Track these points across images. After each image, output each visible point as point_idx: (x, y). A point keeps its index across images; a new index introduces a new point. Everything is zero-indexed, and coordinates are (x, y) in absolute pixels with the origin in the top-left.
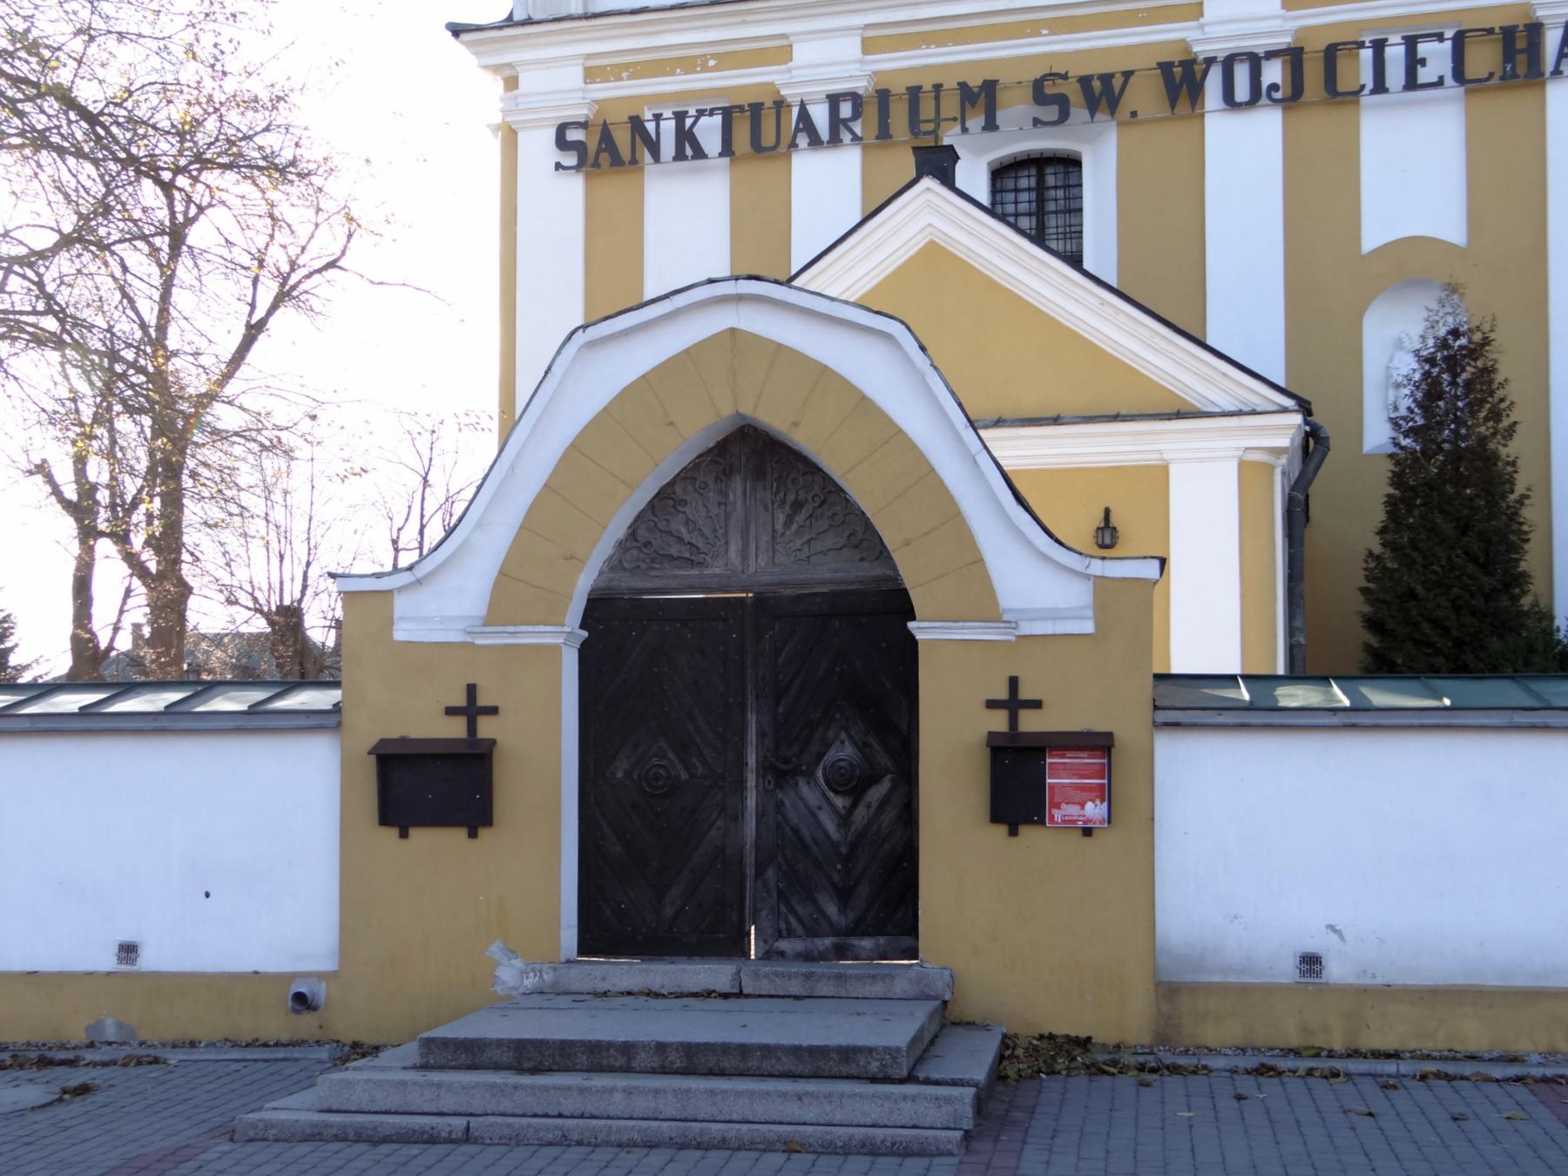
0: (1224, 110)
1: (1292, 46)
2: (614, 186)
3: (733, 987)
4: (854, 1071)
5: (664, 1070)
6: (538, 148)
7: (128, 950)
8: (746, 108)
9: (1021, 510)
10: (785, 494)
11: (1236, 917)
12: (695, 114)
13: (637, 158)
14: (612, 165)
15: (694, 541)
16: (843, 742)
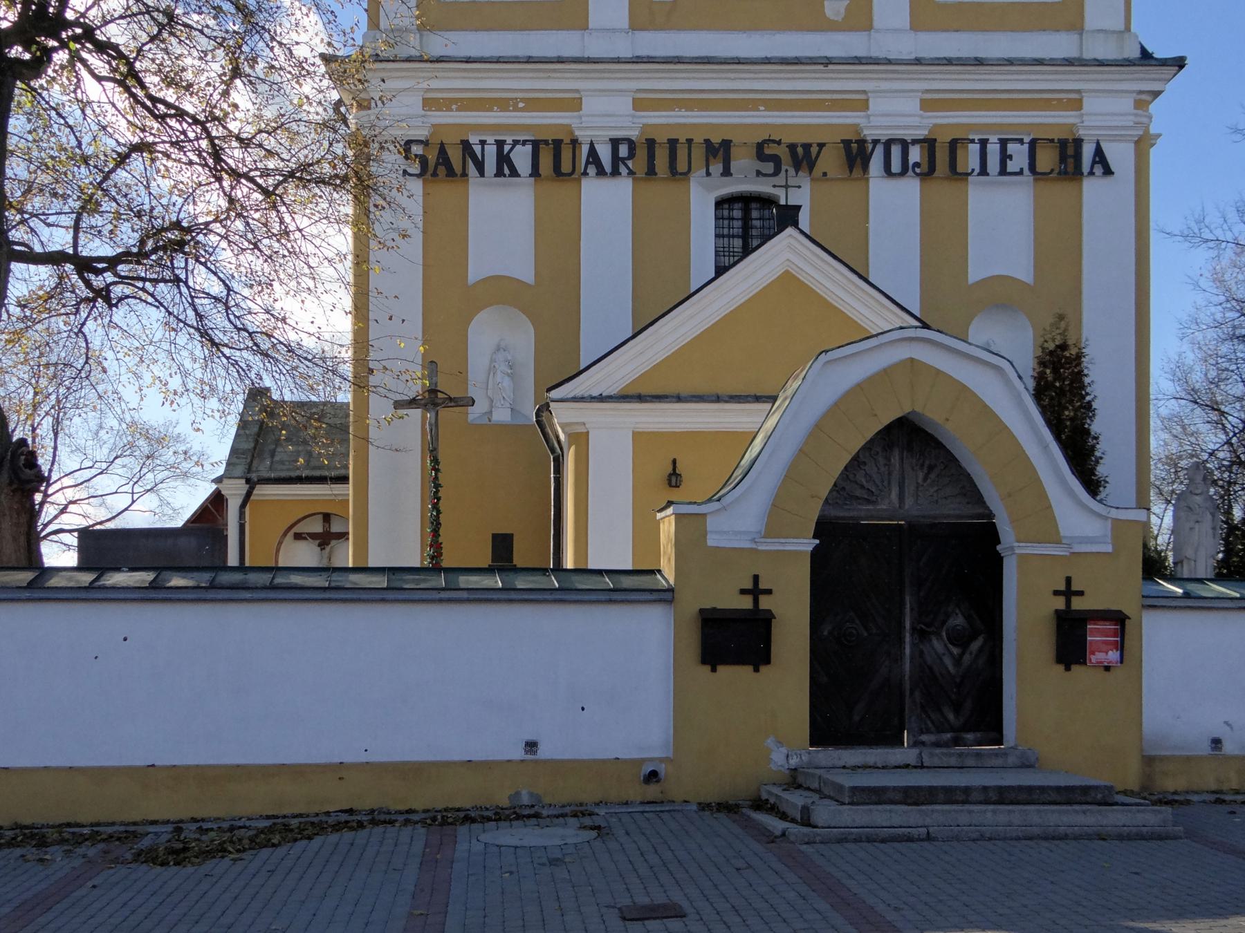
0: (883, 177)
2: (446, 190)
3: (917, 762)
4: (1089, 800)
5: (987, 802)
7: (531, 746)
16: (957, 614)
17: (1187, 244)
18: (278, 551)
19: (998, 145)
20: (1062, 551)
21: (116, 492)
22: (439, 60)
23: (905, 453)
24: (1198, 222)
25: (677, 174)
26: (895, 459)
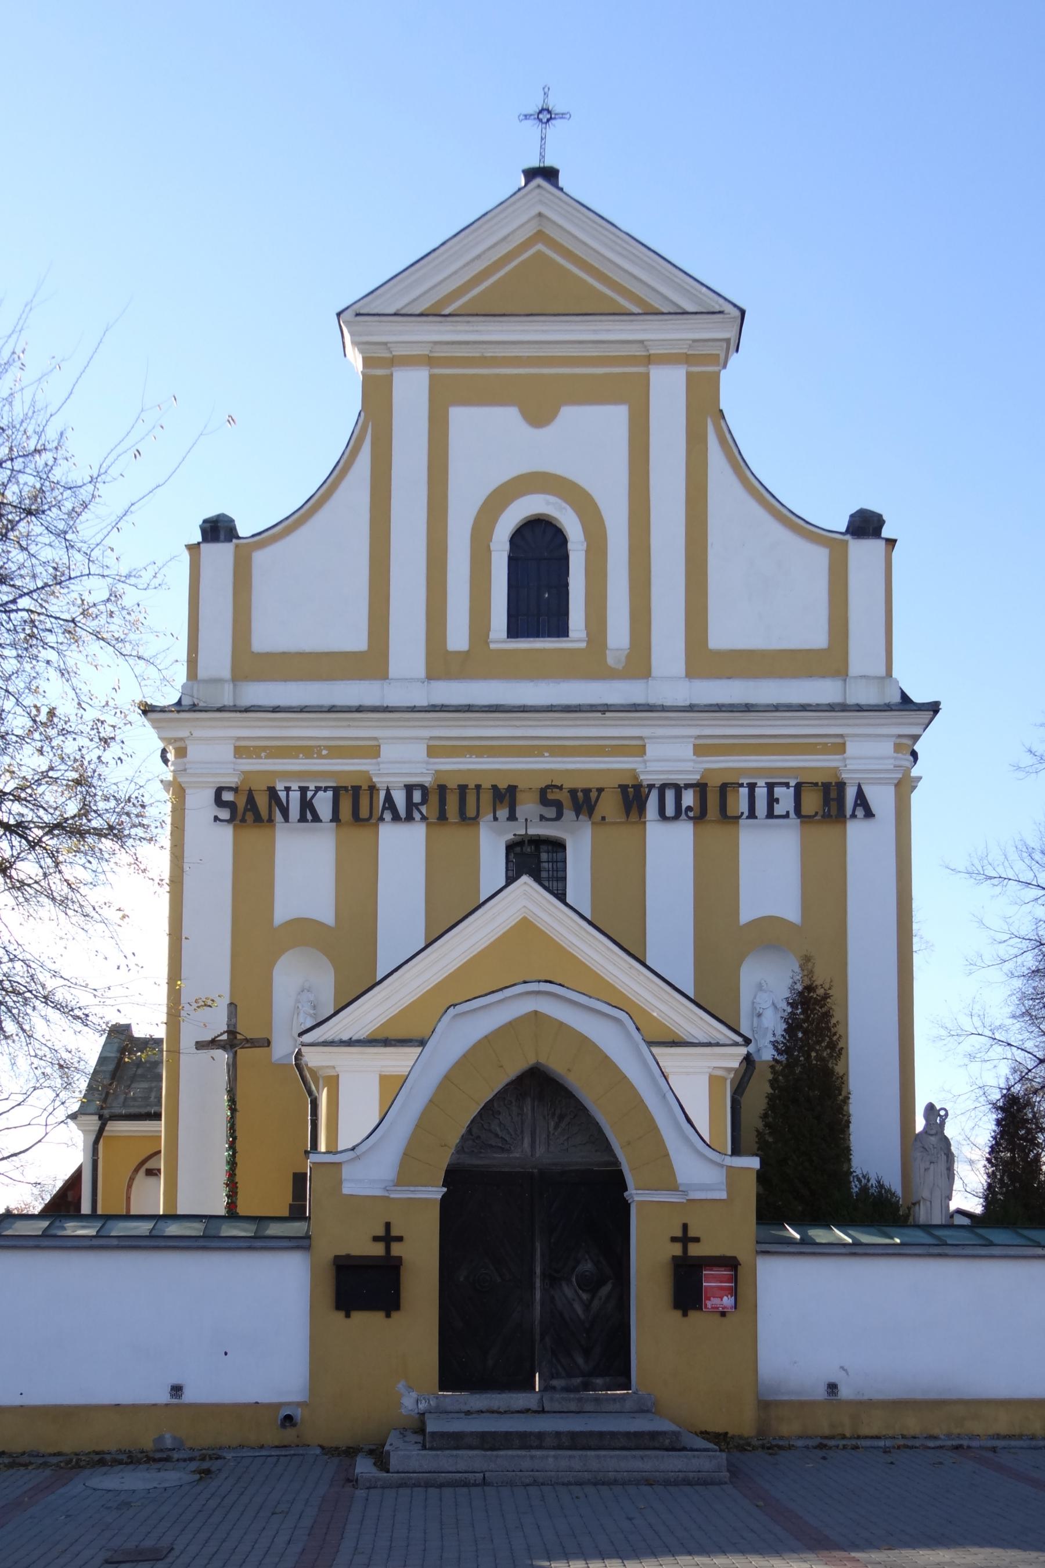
0: (659, 820)
1: (700, 782)
2: (254, 835)
3: (539, 1407)
6: (200, 804)
7: (177, 1390)
8: (350, 788)
9: (689, 1126)
10: (555, 1110)
11: (795, 1363)
12: (314, 789)
13: (273, 818)
14: (255, 821)
15: (504, 1136)
16: (586, 1260)
17: (973, 880)
18: (130, 1186)
19: (766, 789)
20: (678, 1198)
21: (29, 1124)
22: (247, 710)
23: (536, 1104)
24: (981, 860)
25: (469, 820)
26: (527, 1109)
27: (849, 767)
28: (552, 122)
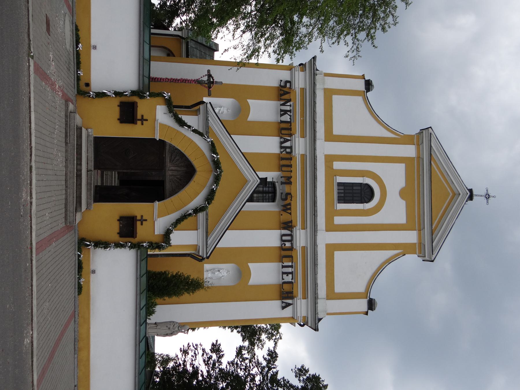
7: (95, 47)
19: (291, 271)
25: (281, 168)
27: (298, 300)
28: (486, 199)
